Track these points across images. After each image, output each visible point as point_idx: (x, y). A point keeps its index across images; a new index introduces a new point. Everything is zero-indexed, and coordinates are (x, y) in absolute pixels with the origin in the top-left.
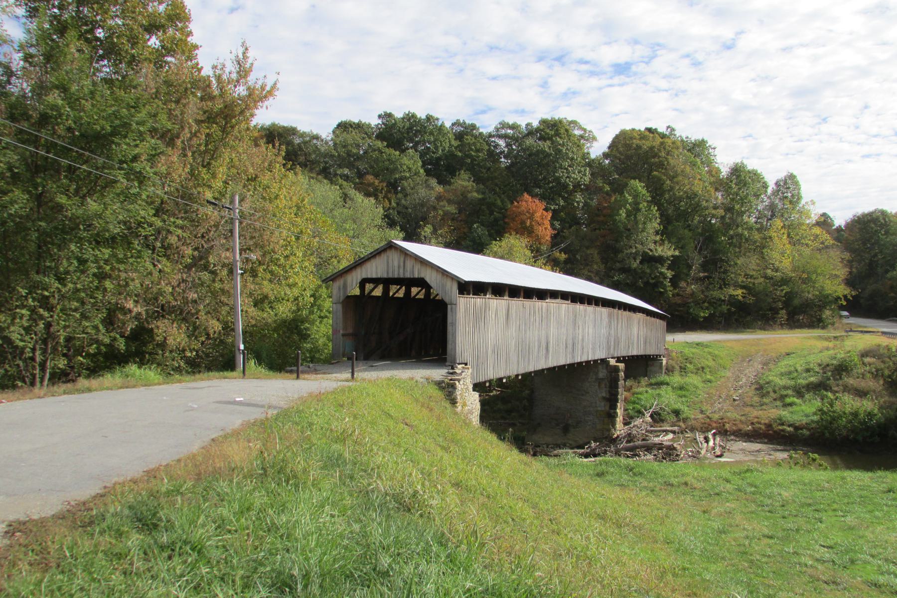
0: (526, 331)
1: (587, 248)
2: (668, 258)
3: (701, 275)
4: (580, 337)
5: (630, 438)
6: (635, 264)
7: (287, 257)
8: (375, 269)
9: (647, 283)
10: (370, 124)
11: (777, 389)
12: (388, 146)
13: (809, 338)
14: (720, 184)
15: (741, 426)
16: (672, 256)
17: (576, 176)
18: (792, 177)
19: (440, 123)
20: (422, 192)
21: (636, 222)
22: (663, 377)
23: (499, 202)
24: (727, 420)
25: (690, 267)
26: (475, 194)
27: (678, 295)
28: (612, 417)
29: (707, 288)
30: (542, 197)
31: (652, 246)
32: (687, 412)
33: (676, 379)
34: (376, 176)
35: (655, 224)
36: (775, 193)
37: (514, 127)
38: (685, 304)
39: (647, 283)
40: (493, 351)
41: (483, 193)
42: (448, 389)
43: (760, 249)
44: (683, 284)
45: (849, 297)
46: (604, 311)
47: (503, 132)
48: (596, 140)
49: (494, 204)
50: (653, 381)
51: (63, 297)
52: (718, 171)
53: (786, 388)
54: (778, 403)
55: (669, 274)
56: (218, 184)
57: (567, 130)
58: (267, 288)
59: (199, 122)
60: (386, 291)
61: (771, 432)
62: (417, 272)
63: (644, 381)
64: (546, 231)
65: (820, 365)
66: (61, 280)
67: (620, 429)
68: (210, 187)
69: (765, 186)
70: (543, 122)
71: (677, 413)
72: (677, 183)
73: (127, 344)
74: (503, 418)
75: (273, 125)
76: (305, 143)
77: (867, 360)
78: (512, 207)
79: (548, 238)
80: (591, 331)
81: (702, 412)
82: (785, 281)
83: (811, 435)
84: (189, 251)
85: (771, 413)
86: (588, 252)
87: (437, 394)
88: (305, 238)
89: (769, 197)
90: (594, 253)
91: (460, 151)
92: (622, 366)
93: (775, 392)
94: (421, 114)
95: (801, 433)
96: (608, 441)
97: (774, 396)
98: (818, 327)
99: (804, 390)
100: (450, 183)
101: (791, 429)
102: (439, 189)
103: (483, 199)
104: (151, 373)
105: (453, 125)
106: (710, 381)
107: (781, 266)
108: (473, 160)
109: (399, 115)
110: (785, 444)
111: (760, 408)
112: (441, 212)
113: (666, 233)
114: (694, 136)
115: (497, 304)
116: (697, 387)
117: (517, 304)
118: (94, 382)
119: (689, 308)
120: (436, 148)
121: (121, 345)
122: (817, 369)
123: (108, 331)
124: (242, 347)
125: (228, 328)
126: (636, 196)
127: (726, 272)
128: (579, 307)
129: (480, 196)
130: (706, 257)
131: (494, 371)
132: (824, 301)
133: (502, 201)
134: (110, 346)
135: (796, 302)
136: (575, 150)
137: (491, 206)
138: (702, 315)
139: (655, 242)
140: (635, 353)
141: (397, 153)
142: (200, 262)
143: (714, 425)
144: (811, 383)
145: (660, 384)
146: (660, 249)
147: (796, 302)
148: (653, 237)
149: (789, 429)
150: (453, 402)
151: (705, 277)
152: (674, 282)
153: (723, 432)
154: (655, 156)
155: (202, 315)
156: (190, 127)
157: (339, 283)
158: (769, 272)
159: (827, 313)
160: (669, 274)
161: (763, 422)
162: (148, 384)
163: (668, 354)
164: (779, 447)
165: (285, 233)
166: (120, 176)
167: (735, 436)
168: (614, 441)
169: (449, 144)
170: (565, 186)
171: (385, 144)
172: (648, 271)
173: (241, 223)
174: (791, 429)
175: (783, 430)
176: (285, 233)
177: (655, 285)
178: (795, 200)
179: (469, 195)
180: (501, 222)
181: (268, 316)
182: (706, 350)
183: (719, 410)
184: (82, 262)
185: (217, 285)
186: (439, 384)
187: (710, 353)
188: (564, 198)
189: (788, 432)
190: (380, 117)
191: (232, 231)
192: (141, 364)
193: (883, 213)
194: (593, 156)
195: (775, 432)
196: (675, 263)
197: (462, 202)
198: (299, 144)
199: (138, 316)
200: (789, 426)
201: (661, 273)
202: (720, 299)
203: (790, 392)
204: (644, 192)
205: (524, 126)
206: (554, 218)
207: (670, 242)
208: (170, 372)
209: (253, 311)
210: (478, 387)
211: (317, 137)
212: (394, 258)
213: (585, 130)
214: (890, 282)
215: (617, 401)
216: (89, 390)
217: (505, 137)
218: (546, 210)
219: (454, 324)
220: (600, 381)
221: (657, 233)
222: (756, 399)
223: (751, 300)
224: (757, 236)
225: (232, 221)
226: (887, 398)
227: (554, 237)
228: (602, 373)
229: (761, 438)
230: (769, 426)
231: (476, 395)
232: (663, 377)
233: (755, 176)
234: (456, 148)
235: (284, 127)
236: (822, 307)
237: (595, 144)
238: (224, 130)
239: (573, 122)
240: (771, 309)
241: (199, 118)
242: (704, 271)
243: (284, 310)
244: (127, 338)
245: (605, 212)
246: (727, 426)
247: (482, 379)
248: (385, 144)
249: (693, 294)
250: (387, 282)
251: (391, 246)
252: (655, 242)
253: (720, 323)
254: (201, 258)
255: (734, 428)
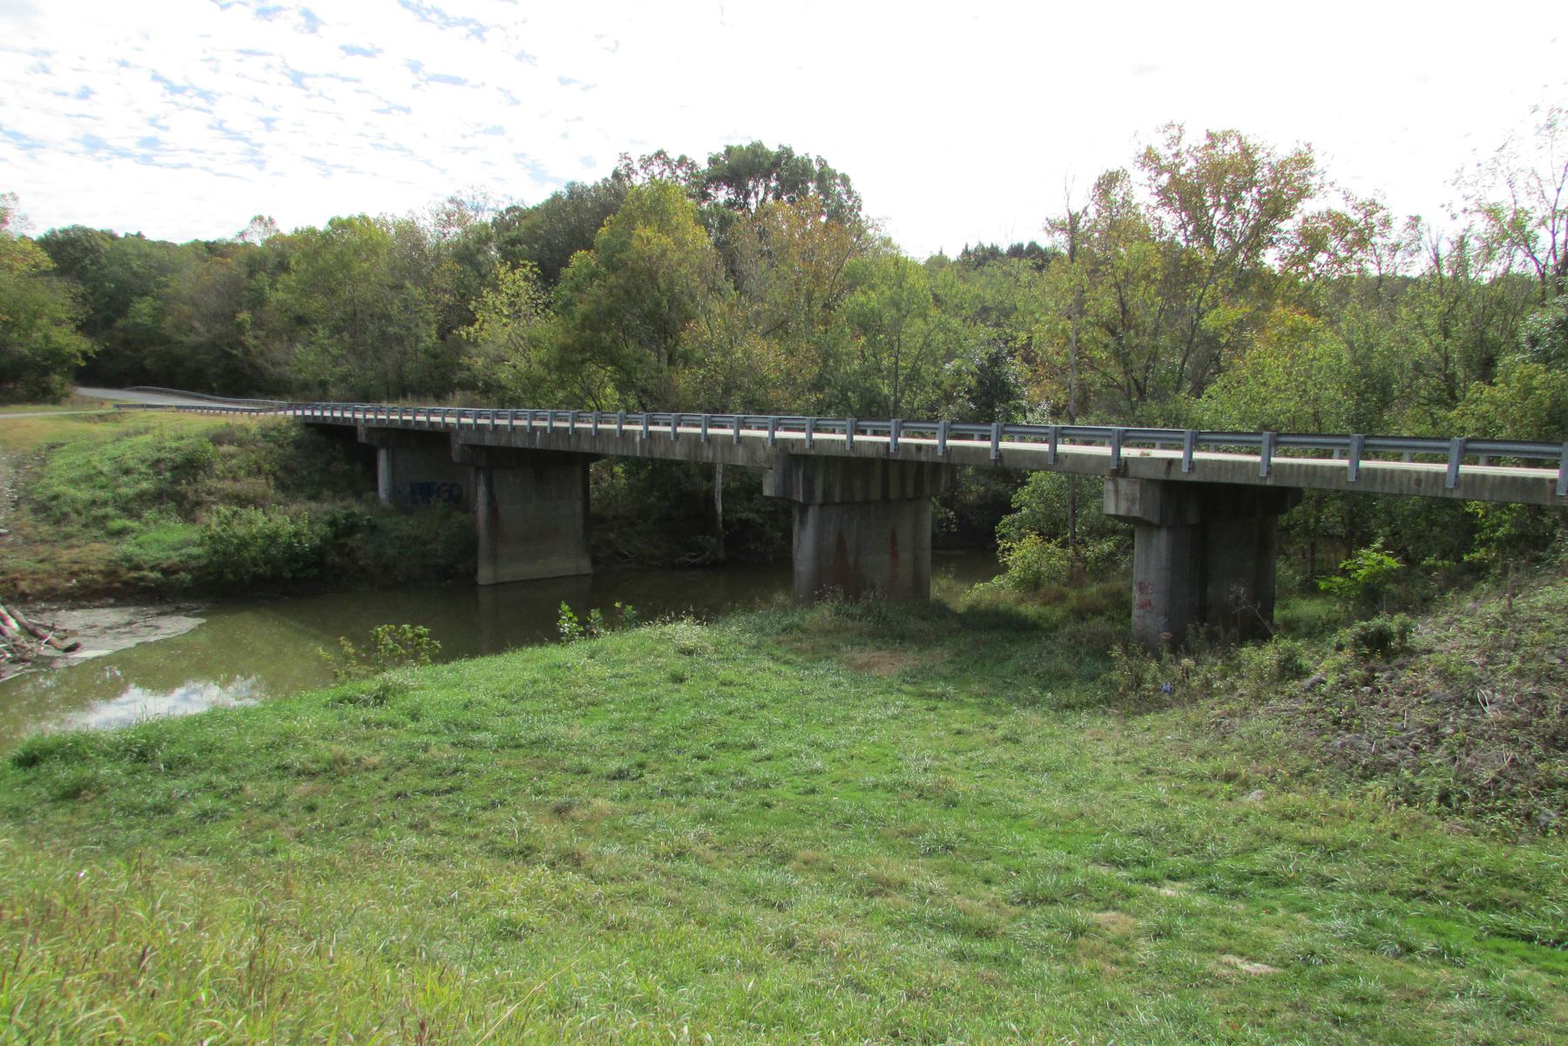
10: (312, 231)
11: (79, 506)
24: (17, 575)
45: (91, 353)
54: (95, 532)
61: (117, 585)
85: (97, 553)
95: (177, 579)
98: (46, 402)
99: (135, 505)
111: (65, 544)
132: (55, 359)
149: (152, 575)
159: (56, 379)
161: (92, 568)
164: (166, 608)
167: (45, 601)
175: (142, 579)
189: (153, 580)
195: (126, 583)
200: (152, 569)
203: (110, 510)
214: (121, 334)
229: (100, 598)
230: (111, 574)
236: (46, 371)
246: (24, 585)
255: (39, 587)
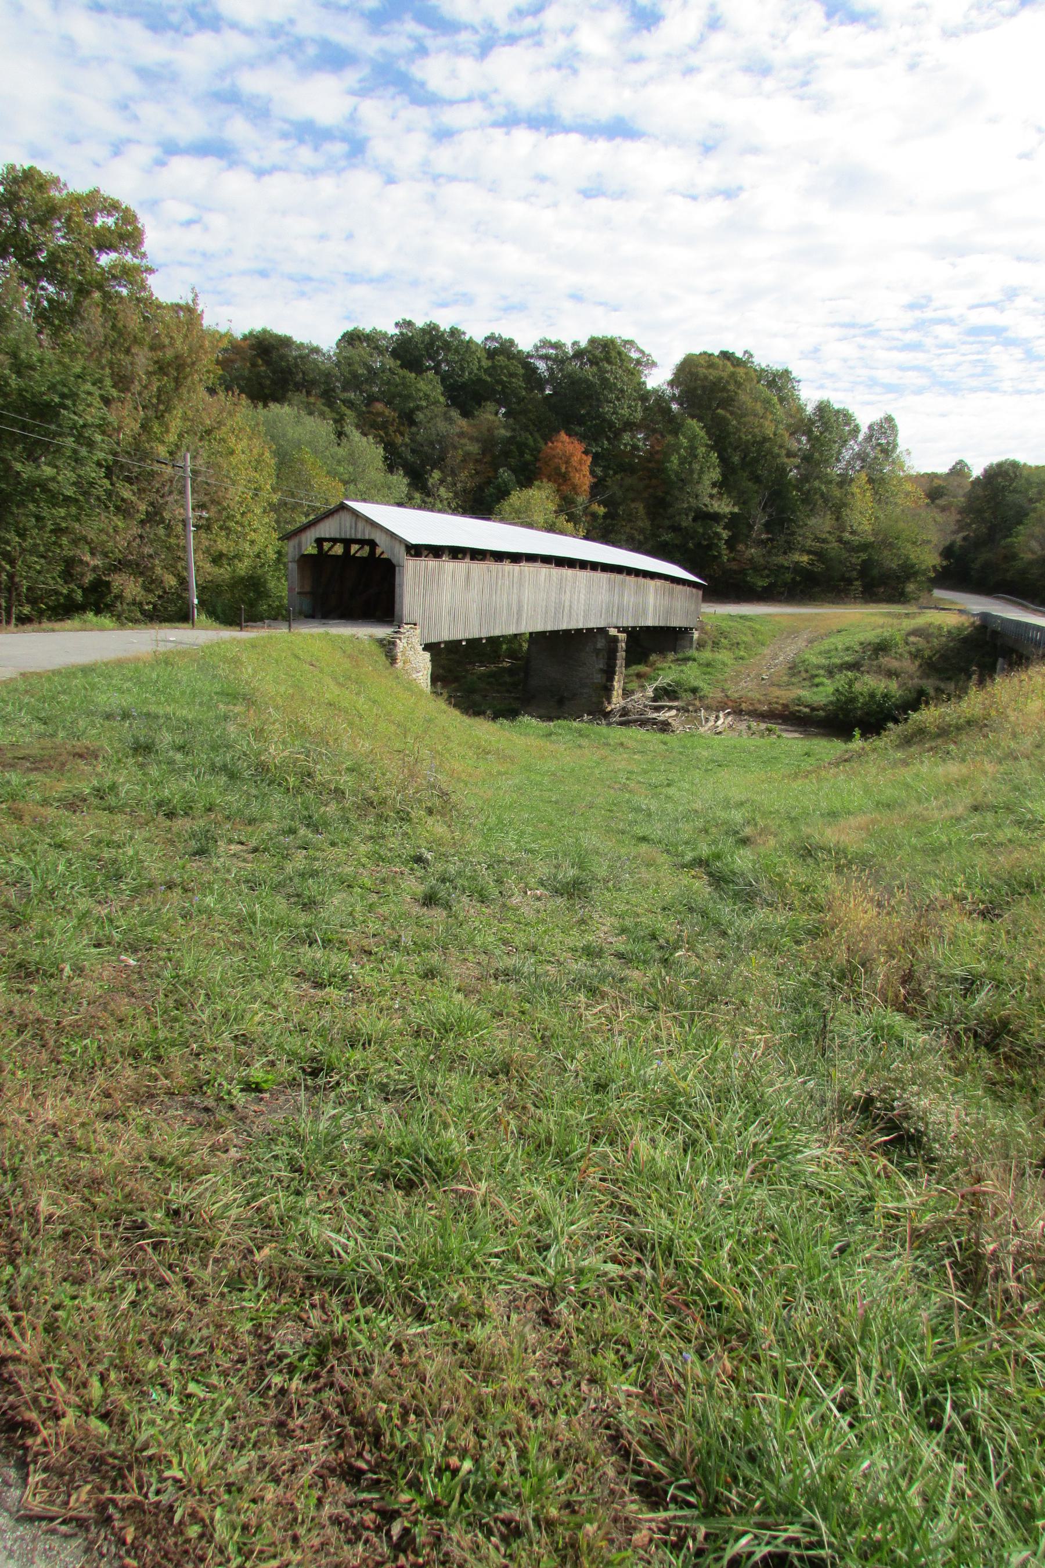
0: (491, 595)
1: (633, 500)
2: (725, 516)
3: (764, 536)
4: (567, 604)
5: (624, 712)
6: (686, 522)
7: (243, 514)
8: (328, 529)
9: (699, 545)
12: (402, 366)
13: (875, 614)
14: (802, 425)
15: (758, 706)
16: (731, 513)
17: (625, 412)
18: (889, 419)
19: (467, 338)
20: (442, 426)
21: (691, 471)
22: (693, 653)
23: (531, 442)
25: (751, 527)
26: (503, 431)
27: (734, 559)
28: (608, 690)
29: (769, 552)
30: (582, 438)
31: (707, 500)
32: (706, 689)
33: (706, 655)
34: (389, 403)
35: (715, 475)
36: (869, 438)
37: (557, 346)
38: (742, 572)
39: (699, 545)
40: (449, 613)
41: (514, 430)
42: (388, 648)
43: (838, 509)
44: (741, 547)
46: (604, 577)
47: (544, 351)
48: (654, 364)
49: (526, 445)
50: (680, 656)
51: (23, 550)
52: (801, 409)
53: (819, 667)
54: (807, 683)
55: (725, 534)
56: (172, 438)
57: (619, 353)
58: (222, 545)
59: (149, 374)
60: (347, 549)
62: (368, 534)
63: (671, 656)
64: (583, 478)
65: (861, 644)
66: (22, 534)
67: (617, 701)
68: (163, 442)
69: (856, 430)
70: (593, 341)
71: (694, 690)
72: (745, 424)
73: (84, 595)
74: (508, 691)
75: (265, 331)
76: (302, 357)
77: (912, 639)
78: (547, 448)
79: (586, 487)
80: (582, 596)
81: (723, 690)
82: (865, 547)
83: (827, 716)
84: (143, 507)
86: (633, 505)
87: (375, 648)
88: (263, 494)
89: (860, 444)
90: (640, 507)
91: (490, 375)
92: (623, 636)
93: (807, 671)
94: (445, 326)
96: (600, 713)
97: (804, 675)
100: (473, 417)
101: (807, 710)
102: (463, 423)
103: (513, 437)
104: (106, 621)
105: (486, 339)
106: (742, 658)
107: (860, 529)
108: (504, 387)
109: (420, 323)
110: (799, 725)
112: (460, 452)
113: (724, 485)
114: (777, 367)
115: (450, 566)
116: (725, 664)
117: (478, 568)
118: (58, 625)
119: (746, 575)
120: (462, 369)
121: (79, 596)
122: (857, 648)
123: (66, 582)
124: (196, 601)
125: (183, 582)
126: (692, 439)
127: (793, 534)
128: (568, 572)
129: (508, 434)
130: (770, 516)
131: (445, 634)
132: (908, 572)
133: (535, 440)
134: (69, 597)
135: (875, 572)
136: (625, 379)
137: (522, 447)
138: (760, 584)
139: (711, 496)
140: (650, 623)
141: (413, 375)
142: (154, 516)
143: (730, 704)
144: (846, 663)
145: (687, 659)
146: (716, 504)
147: (875, 572)
148: (709, 490)
150: (393, 660)
151: (769, 539)
152: (731, 544)
153: (738, 712)
154: (724, 389)
155: (159, 571)
156: (140, 381)
157: (294, 542)
158: (847, 536)
159: (911, 587)
160: (725, 534)
162: (102, 629)
163: (702, 629)
165: (241, 489)
166: (70, 441)
168: (607, 715)
169: (475, 367)
170: (611, 425)
171: (399, 362)
172: (701, 530)
173: (193, 481)
174: (807, 710)
176: (241, 489)
177: (709, 547)
178: (887, 451)
179: (496, 432)
180: (532, 467)
181: (223, 573)
182: (748, 623)
183: (746, 689)
184: (39, 518)
185: (173, 541)
186: (381, 642)
187: (750, 628)
188: (608, 439)
190: (397, 325)
191: (185, 486)
192: (98, 612)
193: (1014, 465)
194: (649, 387)
195: (791, 713)
196: (733, 522)
197: (488, 443)
198: (295, 358)
199: (95, 569)
201: (717, 534)
202: (782, 566)
203: (822, 672)
204: (702, 433)
205: (569, 345)
206: (595, 462)
207: (730, 496)
208: (123, 620)
209: (208, 567)
210: (428, 647)
211: (316, 350)
212: (346, 518)
213: (642, 352)
215: (614, 673)
216: (53, 630)
217: (546, 358)
218: (586, 453)
219: (401, 585)
220: (597, 652)
221: (714, 485)
222: (785, 678)
223: (819, 568)
224: (837, 493)
225: (184, 478)
226: (916, 681)
227: (594, 487)
228: (601, 644)
230: (785, 706)
231: (427, 655)
232: (693, 653)
233: (846, 417)
234: (485, 370)
235: (277, 336)
237: (654, 371)
238: (176, 380)
239: (631, 343)
240: (843, 578)
241: (150, 369)
242: (768, 533)
243: (243, 568)
244: (84, 590)
245: (657, 457)
246: (744, 706)
247: (434, 640)
248: (399, 362)
249: (751, 560)
250: (347, 542)
251: (343, 507)
252: (711, 496)
253: (782, 593)
254: (156, 514)
